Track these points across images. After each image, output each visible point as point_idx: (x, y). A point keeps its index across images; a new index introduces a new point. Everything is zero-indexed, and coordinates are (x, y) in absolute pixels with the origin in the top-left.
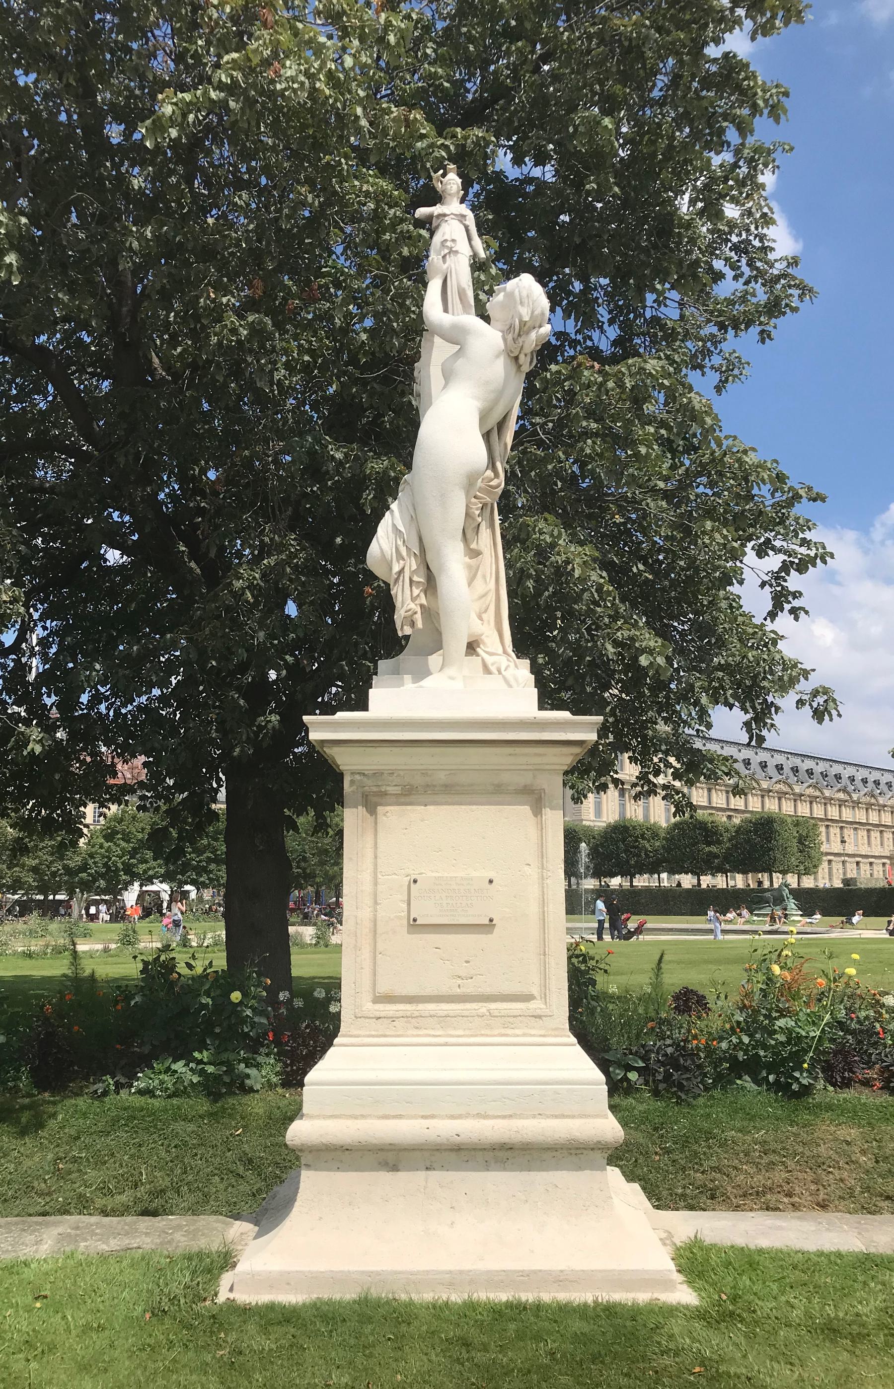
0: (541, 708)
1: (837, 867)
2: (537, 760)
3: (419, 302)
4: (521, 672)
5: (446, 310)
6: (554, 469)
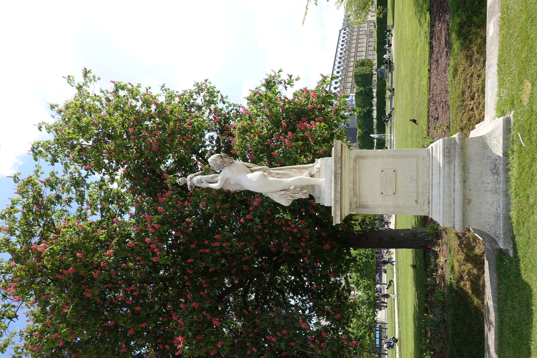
0: (331, 156)
1: (370, 53)
2: (346, 157)
3: (216, 190)
4: (319, 162)
5: (217, 182)
6: (265, 154)
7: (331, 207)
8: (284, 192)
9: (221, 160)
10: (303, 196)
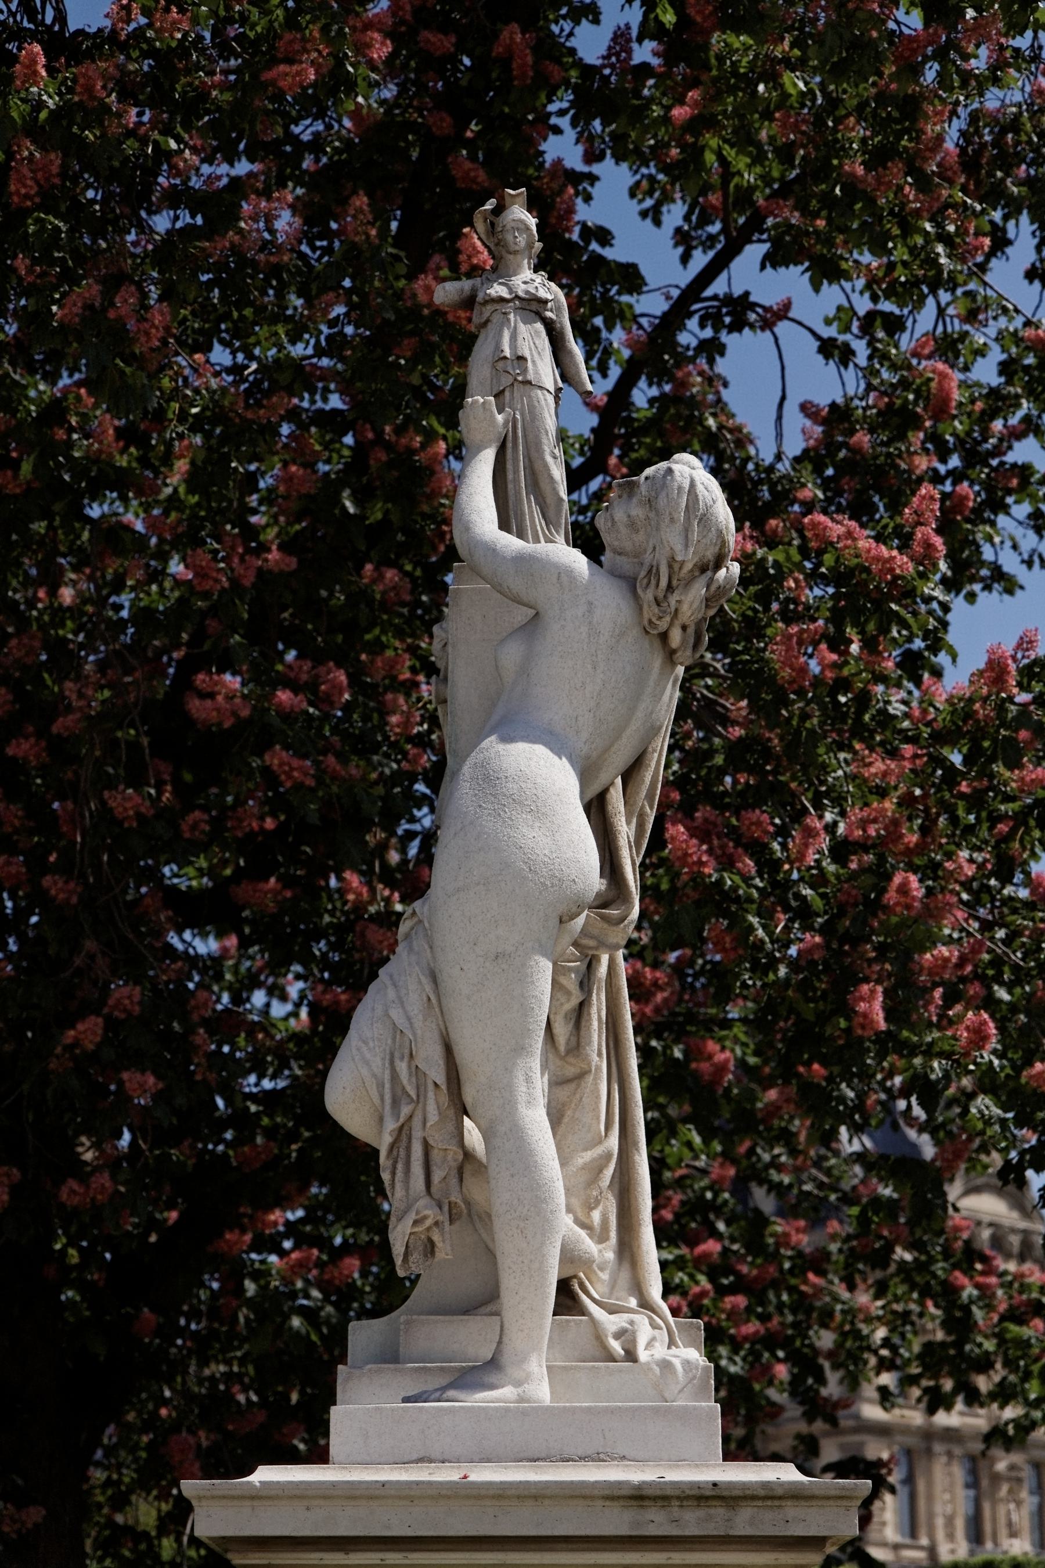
4: (672, 1353)
5: (504, 525)
7: (320, 1456)
8: (437, 1073)
9: (689, 558)
10: (409, 1217)
